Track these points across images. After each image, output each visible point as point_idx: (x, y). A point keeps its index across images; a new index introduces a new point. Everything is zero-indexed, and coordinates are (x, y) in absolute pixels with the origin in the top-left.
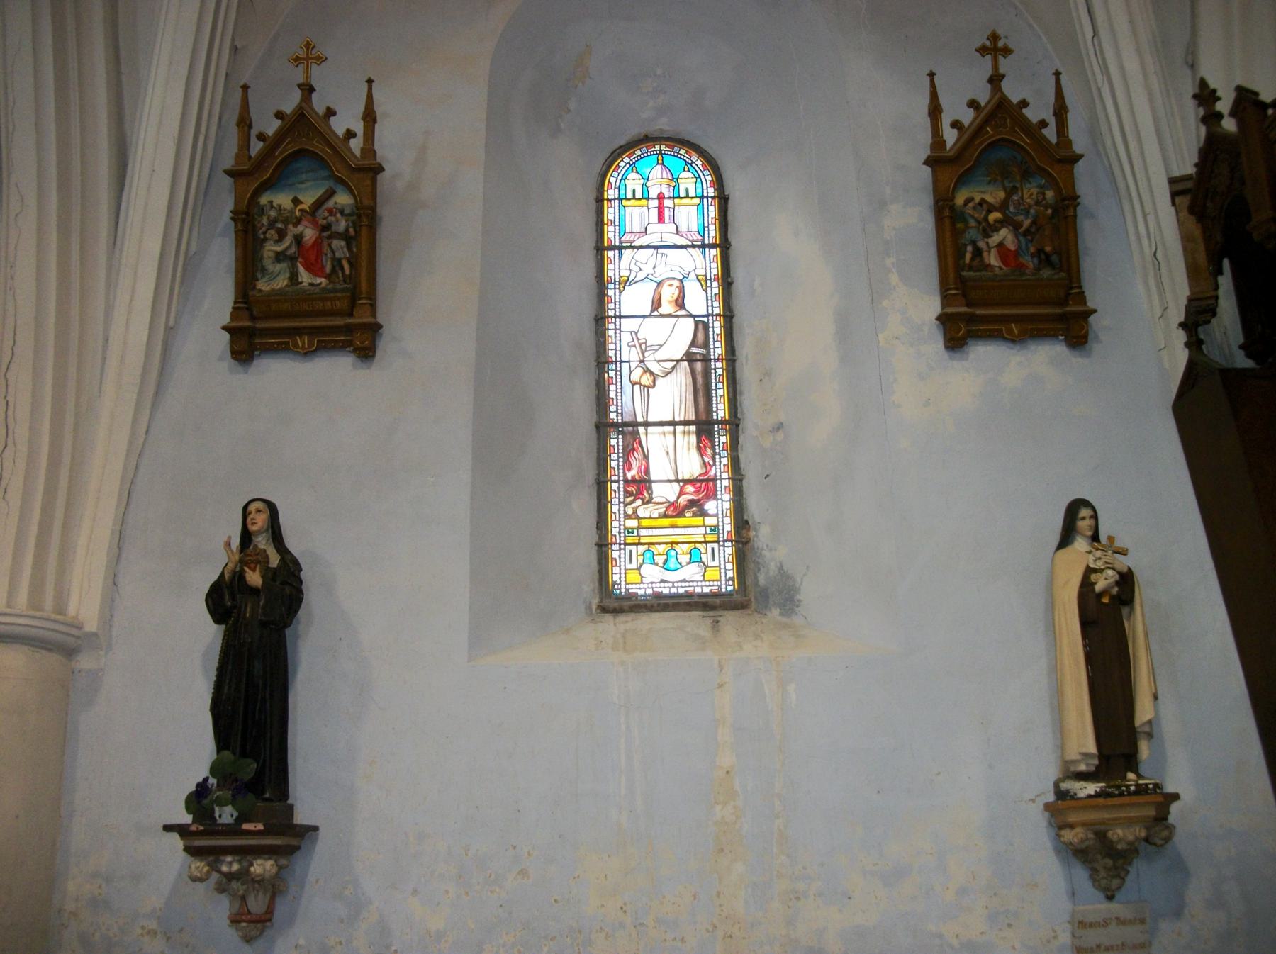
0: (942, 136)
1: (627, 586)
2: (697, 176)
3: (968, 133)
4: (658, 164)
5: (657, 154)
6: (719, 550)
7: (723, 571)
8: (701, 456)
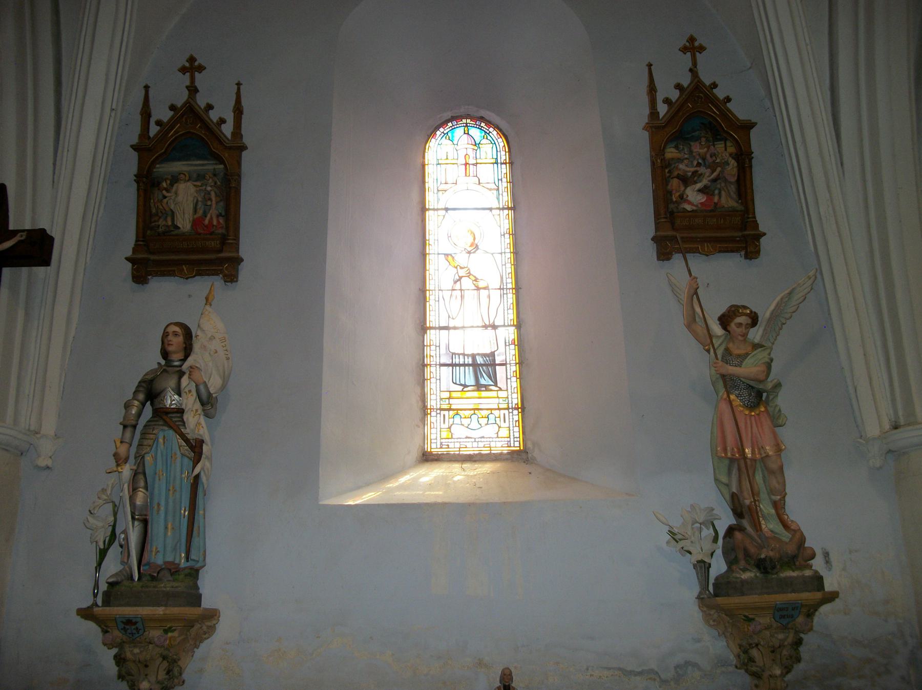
0: (657, 109)
1: (442, 441)
2: (493, 142)
3: (676, 106)
5: (463, 126)
7: (511, 432)
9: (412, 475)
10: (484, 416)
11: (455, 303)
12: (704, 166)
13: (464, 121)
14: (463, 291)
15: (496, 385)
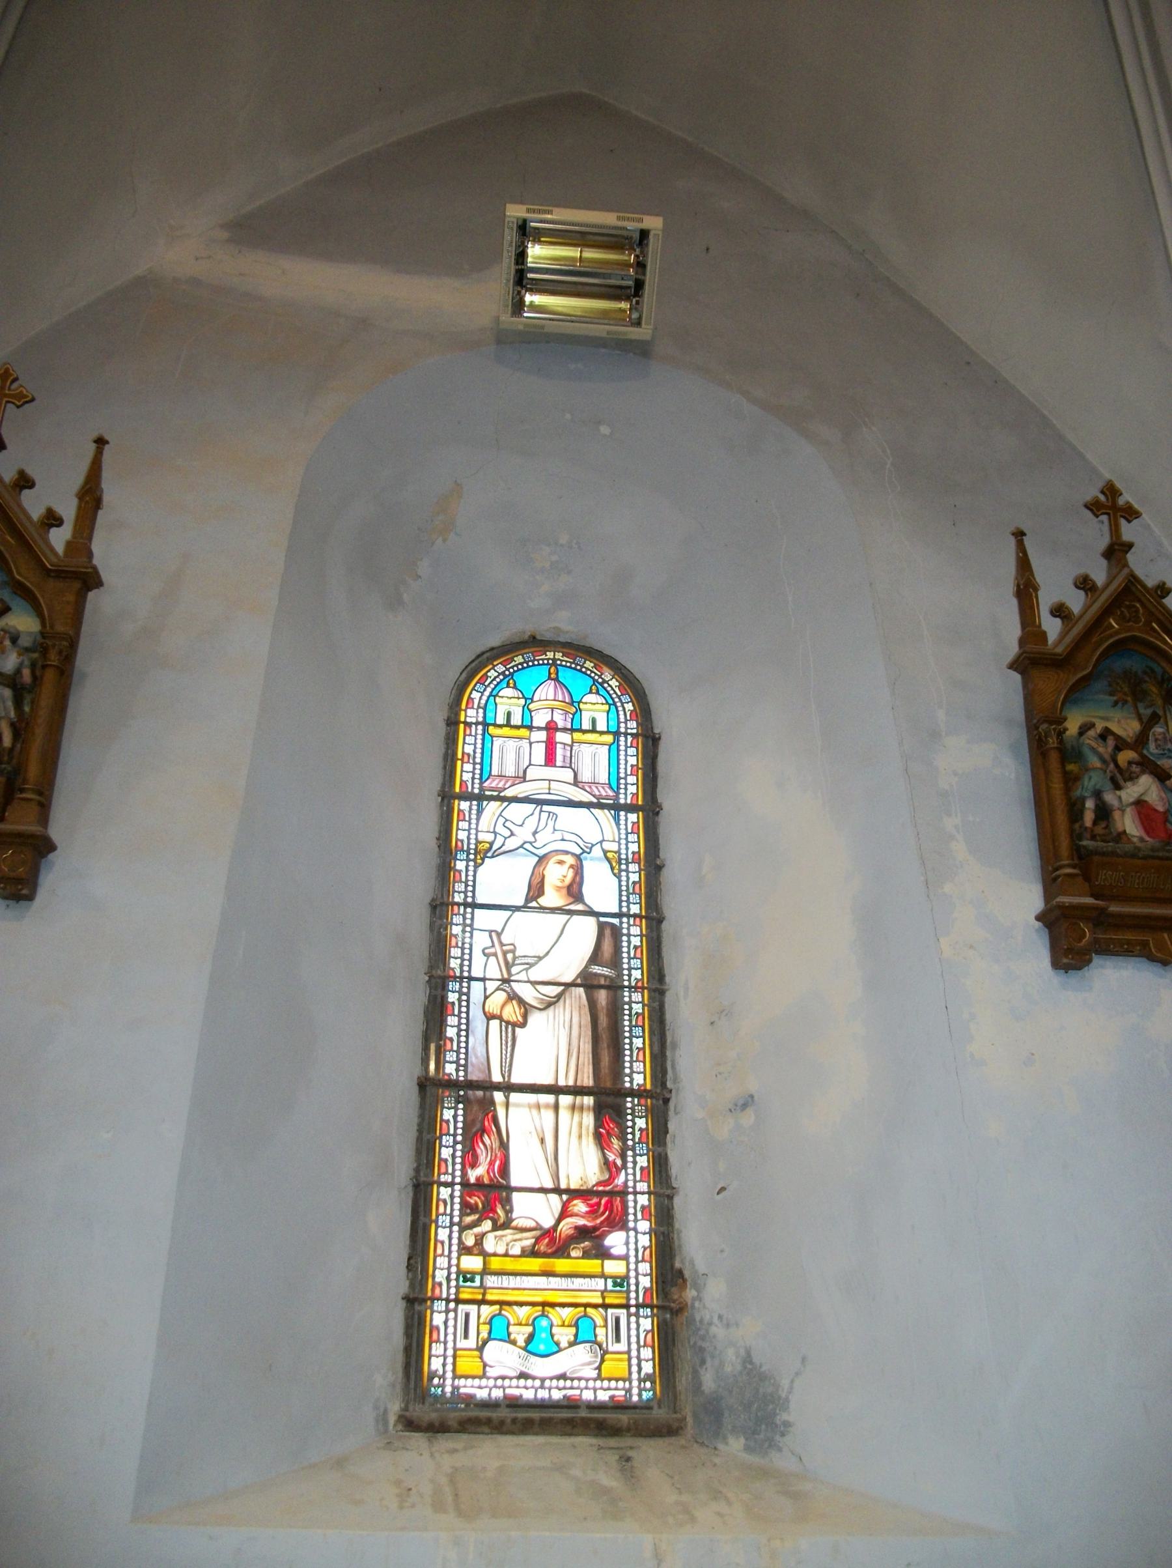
2: (610, 701)
8: (602, 1149)
10: (524, 1322)
13: (550, 655)
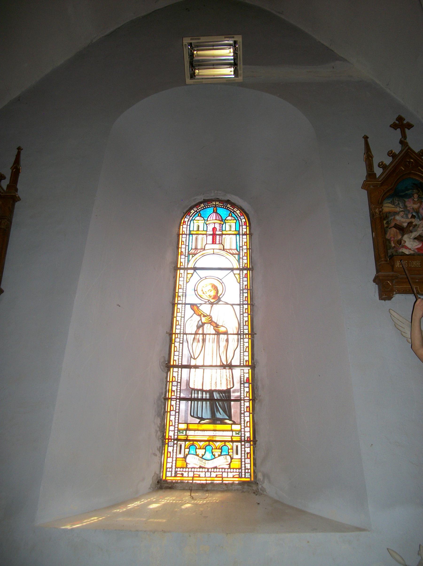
0: (373, 171)
2: (237, 219)
4: (214, 212)
5: (213, 207)
6: (241, 448)
7: (243, 463)
9: (143, 501)
11: (197, 347)
12: (418, 218)
14: (204, 336)
15: (230, 418)
